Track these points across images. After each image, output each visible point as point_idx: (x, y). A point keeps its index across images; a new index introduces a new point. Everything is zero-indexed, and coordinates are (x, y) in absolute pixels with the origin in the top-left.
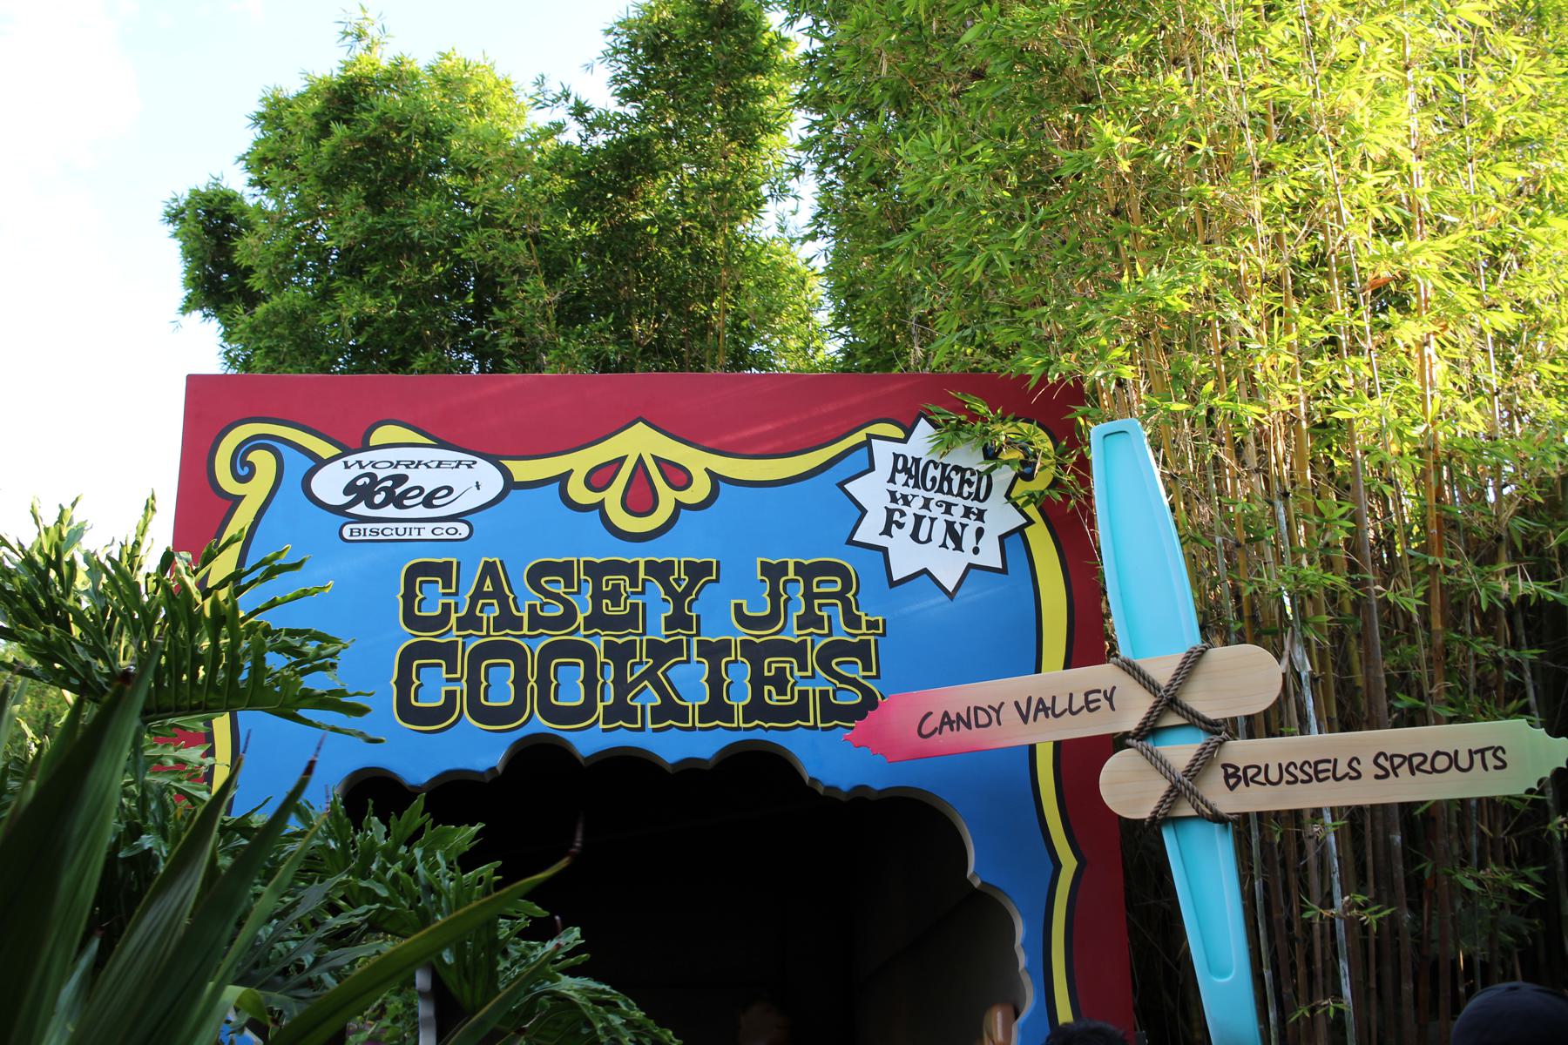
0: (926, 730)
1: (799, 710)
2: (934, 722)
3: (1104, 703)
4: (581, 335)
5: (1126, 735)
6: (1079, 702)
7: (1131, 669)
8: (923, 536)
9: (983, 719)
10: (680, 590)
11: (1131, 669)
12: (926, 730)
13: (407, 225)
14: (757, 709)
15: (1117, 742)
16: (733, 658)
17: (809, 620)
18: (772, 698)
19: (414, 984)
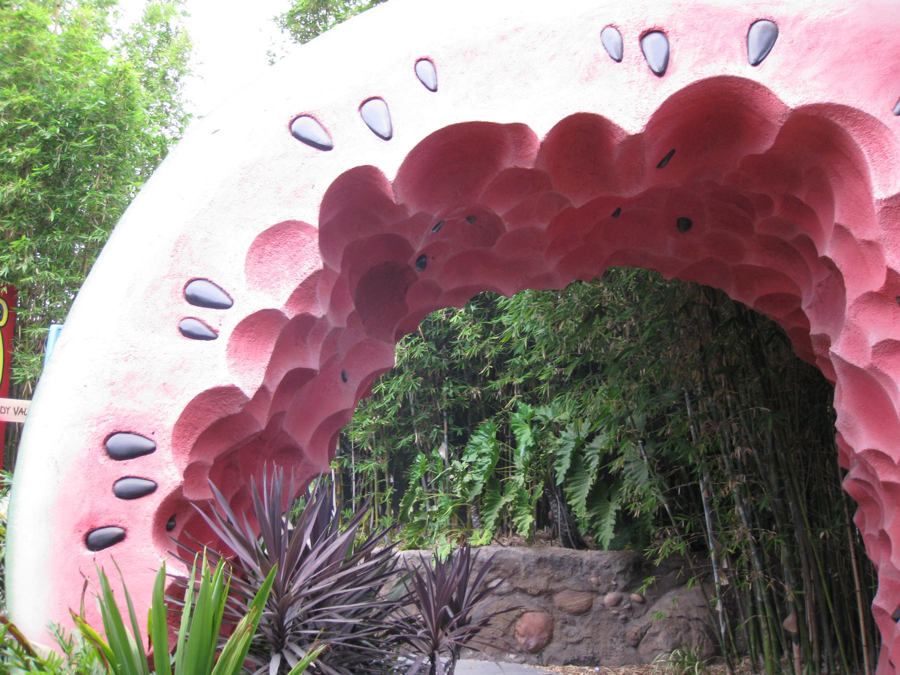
9: (3, 411)
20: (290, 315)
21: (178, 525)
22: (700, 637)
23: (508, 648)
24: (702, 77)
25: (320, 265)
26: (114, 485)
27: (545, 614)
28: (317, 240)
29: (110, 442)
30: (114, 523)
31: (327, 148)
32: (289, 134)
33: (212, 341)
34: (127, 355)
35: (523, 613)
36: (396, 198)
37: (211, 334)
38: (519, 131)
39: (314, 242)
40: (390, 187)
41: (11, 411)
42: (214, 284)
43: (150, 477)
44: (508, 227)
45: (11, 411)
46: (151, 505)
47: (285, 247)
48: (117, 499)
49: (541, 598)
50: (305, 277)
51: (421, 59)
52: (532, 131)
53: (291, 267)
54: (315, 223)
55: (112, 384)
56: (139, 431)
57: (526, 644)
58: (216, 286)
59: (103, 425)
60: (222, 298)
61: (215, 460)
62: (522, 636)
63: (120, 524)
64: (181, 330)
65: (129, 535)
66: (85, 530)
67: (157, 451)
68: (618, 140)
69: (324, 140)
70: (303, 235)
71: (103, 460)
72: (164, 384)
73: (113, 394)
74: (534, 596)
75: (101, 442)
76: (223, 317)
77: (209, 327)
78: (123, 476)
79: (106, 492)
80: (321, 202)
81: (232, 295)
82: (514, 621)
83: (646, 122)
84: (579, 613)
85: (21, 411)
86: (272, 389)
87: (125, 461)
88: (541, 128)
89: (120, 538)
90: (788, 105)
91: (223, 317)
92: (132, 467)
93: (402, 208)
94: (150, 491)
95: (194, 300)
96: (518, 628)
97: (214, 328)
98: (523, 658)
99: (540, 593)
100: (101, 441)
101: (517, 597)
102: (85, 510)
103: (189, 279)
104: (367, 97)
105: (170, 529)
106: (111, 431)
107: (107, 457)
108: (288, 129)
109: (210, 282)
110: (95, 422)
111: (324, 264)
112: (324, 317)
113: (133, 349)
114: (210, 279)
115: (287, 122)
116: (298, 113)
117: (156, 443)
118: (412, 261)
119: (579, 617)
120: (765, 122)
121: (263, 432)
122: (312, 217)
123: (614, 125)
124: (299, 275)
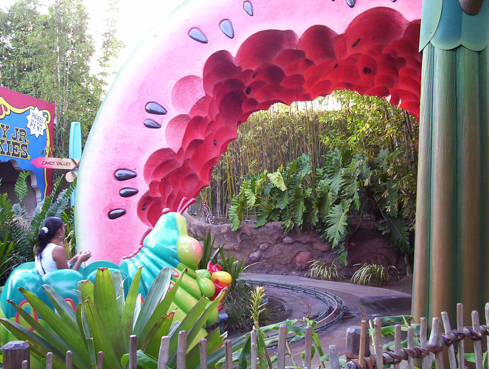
0: (43, 164)
1: (18, 155)
2: (45, 162)
3: (68, 165)
4: (361, 177)
5: (70, 170)
6: (65, 164)
7: (73, 160)
8: (35, 128)
9: (52, 164)
10: (15, 127)
11: (73, 160)
12: (43, 164)
13: (405, 222)
14: (13, 154)
15: (68, 171)
16: (5, 143)
17: (21, 140)
18: (16, 153)
19: (203, 140)
20: (192, 117)
21: (147, 208)
22: (382, 262)
23: (293, 268)
24: (370, 8)
25: (204, 95)
26: (120, 191)
27: (309, 253)
28: (202, 84)
29: (116, 174)
30: (120, 207)
31: (206, 42)
32: (188, 36)
33: (158, 129)
34: (122, 136)
35: (299, 252)
36: (237, 65)
37: (158, 126)
38: (290, 34)
39: (201, 85)
40: (234, 59)
41: (56, 164)
42: (158, 104)
43: (135, 188)
44: (287, 74)
45: (56, 164)
46: (136, 199)
47: (189, 87)
48: (121, 197)
49: (308, 245)
50: (198, 100)
51: (246, 1)
52: (295, 33)
53: (191, 95)
54: (201, 76)
55: (116, 149)
56: (129, 168)
57: (301, 267)
58: (159, 105)
59: (113, 167)
60: (161, 110)
61: (161, 180)
62: (299, 263)
63: (123, 208)
64: (145, 124)
65: (127, 211)
66: (108, 211)
67: (137, 177)
68: (332, 37)
69: (204, 39)
70: (196, 81)
71: (114, 181)
72: (139, 148)
73: (117, 153)
74: (304, 244)
75: (113, 174)
76: (163, 118)
77: (157, 123)
78: (123, 187)
79: (116, 195)
80: (203, 67)
81: (166, 109)
82: (295, 256)
83: (345, 28)
84: (325, 252)
85: (60, 163)
86: (185, 149)
87: (124, 181)
88: (300, 30)
89: (123, 213)
90: (408, 20)
91: (163, 118)
92: (127, 184)
93: (240, 68)
94: (136, 193)
95: (151, 112)
96: (297, 259)
97: (159, 123)
98: (300, 274)
99: (307, 243)
100: (112, 173)
101: (296, 245)
102: (108, 202)
103: (147, 102)
104: (222, 19)
105: (144, 209)
106: (117, 168)
107: (116, 180)
108: (188, 34)
109: (156, 103)
110: (110, 165)
111: (206, 94)
112: (206, 117)
113: (124, 133)
114: (156, 102)
115: (187, 31)
116: (192, 27)
117: (136, 174)
118: (244, 91)
119: (325, 254)
120: (399, 27)
121: (181, 168)
122: (200, 74)
123: (332, 30)
124: (195, 99)
